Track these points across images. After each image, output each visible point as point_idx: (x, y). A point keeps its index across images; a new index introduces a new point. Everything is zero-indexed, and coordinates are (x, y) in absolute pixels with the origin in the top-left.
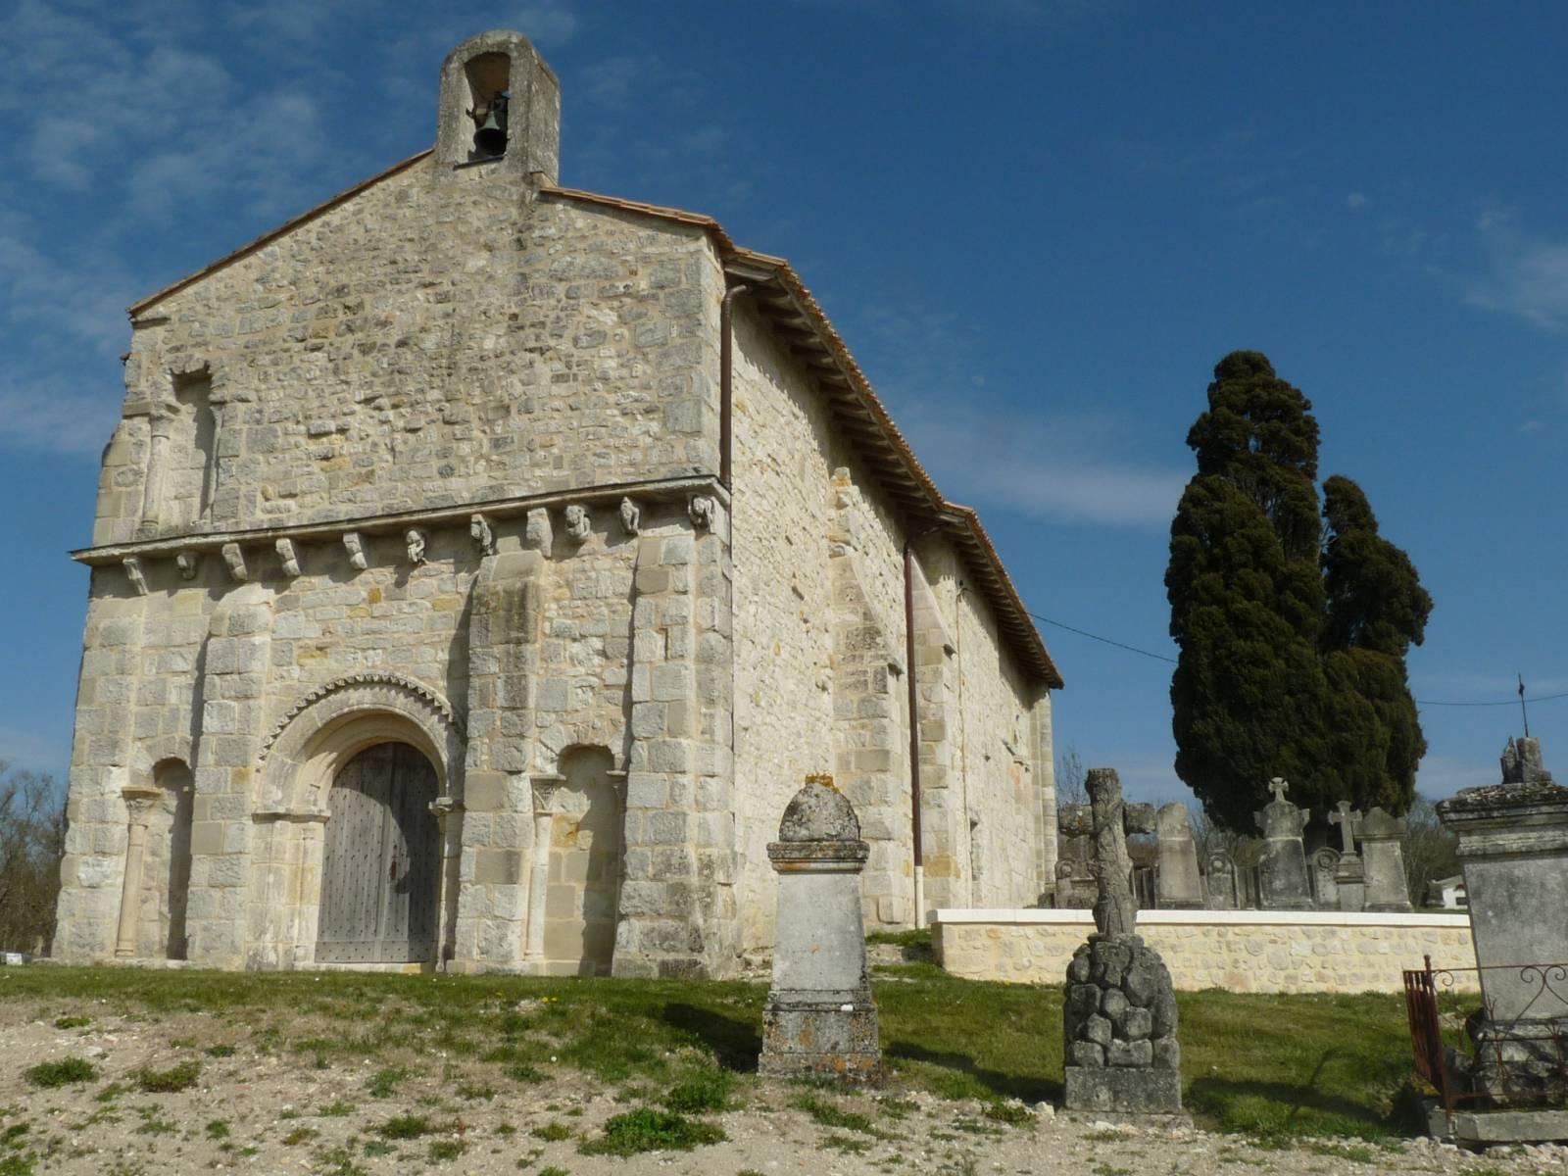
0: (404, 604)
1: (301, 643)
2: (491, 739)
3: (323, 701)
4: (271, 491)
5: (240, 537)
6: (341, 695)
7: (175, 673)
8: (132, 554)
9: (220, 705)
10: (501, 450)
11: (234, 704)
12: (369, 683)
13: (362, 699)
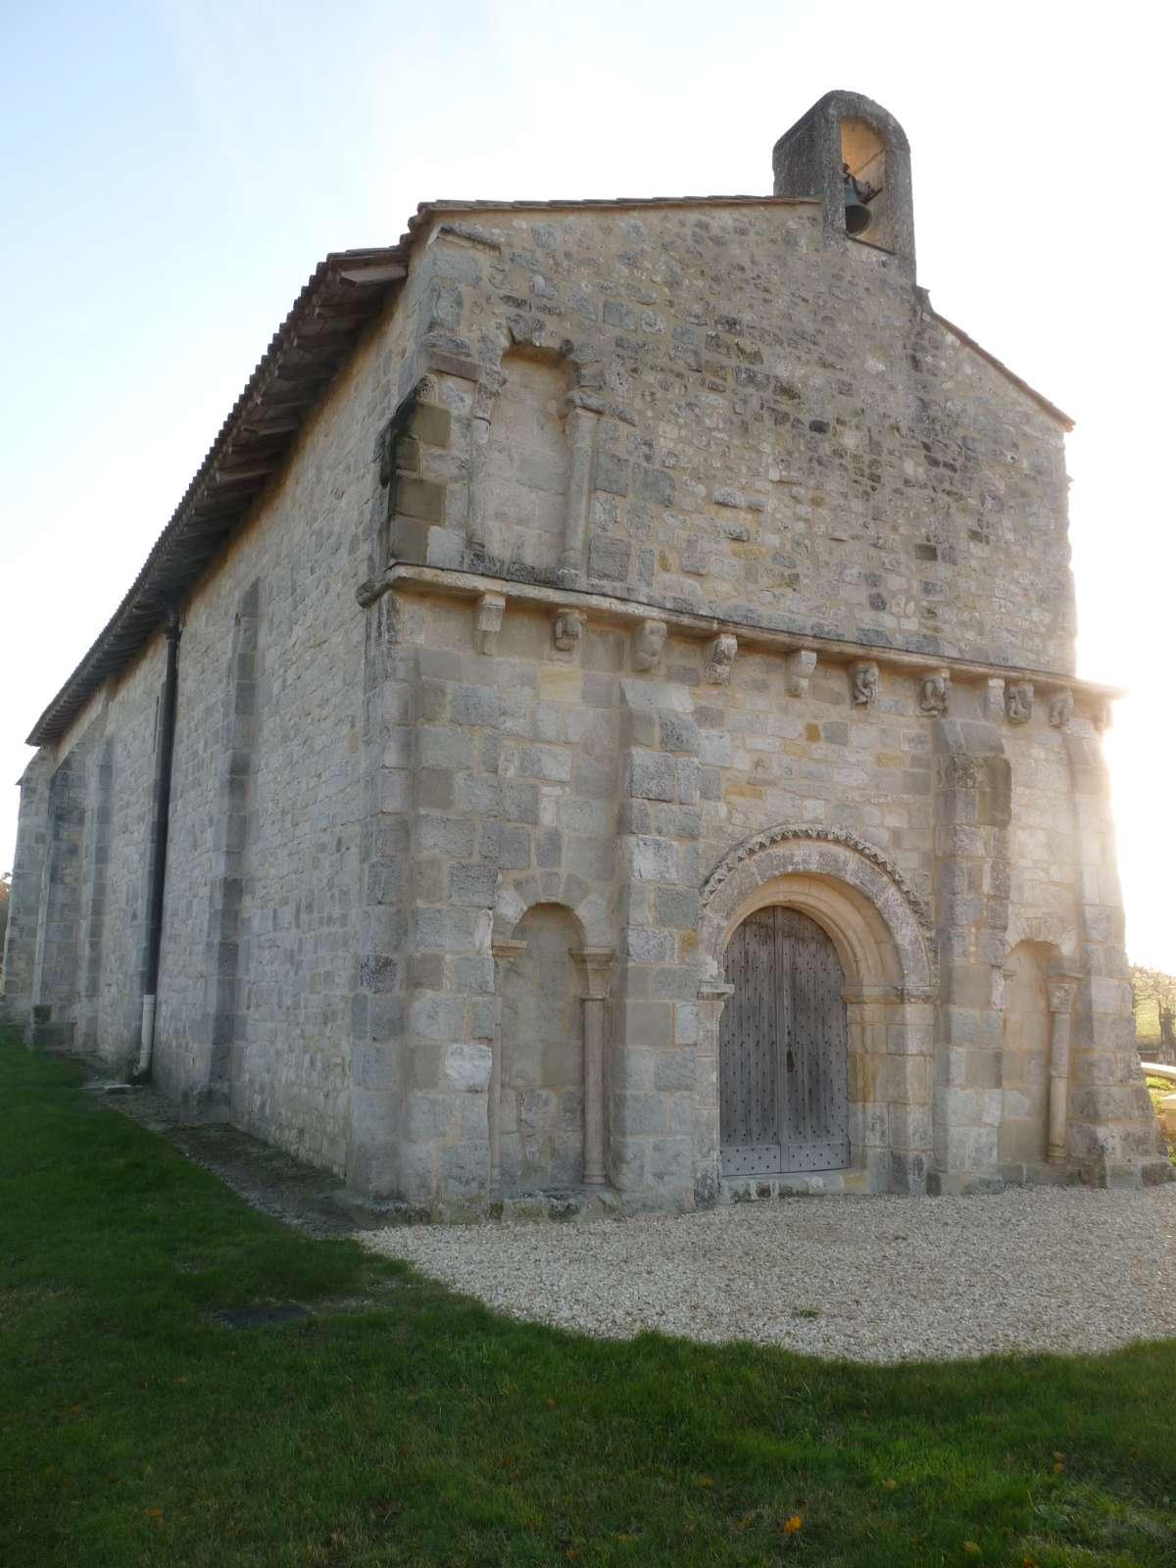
0: (846, 751)
1: (728, 774)
2: (978, 928)
3: (762, 854)
4: (673, 558)
5: (674, 619)
6: (779, 850)
7: (548, 781)
8: (500, 594)
9: (658, 844)
10: (931, 598)
11: (675, 843)
12: (822, 837)
13: (806, 855)
